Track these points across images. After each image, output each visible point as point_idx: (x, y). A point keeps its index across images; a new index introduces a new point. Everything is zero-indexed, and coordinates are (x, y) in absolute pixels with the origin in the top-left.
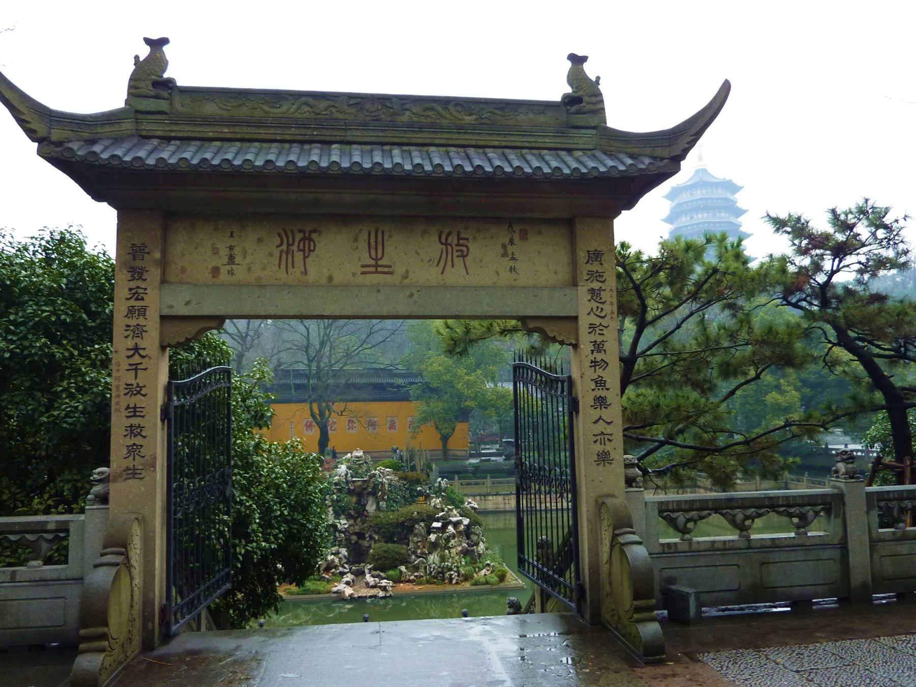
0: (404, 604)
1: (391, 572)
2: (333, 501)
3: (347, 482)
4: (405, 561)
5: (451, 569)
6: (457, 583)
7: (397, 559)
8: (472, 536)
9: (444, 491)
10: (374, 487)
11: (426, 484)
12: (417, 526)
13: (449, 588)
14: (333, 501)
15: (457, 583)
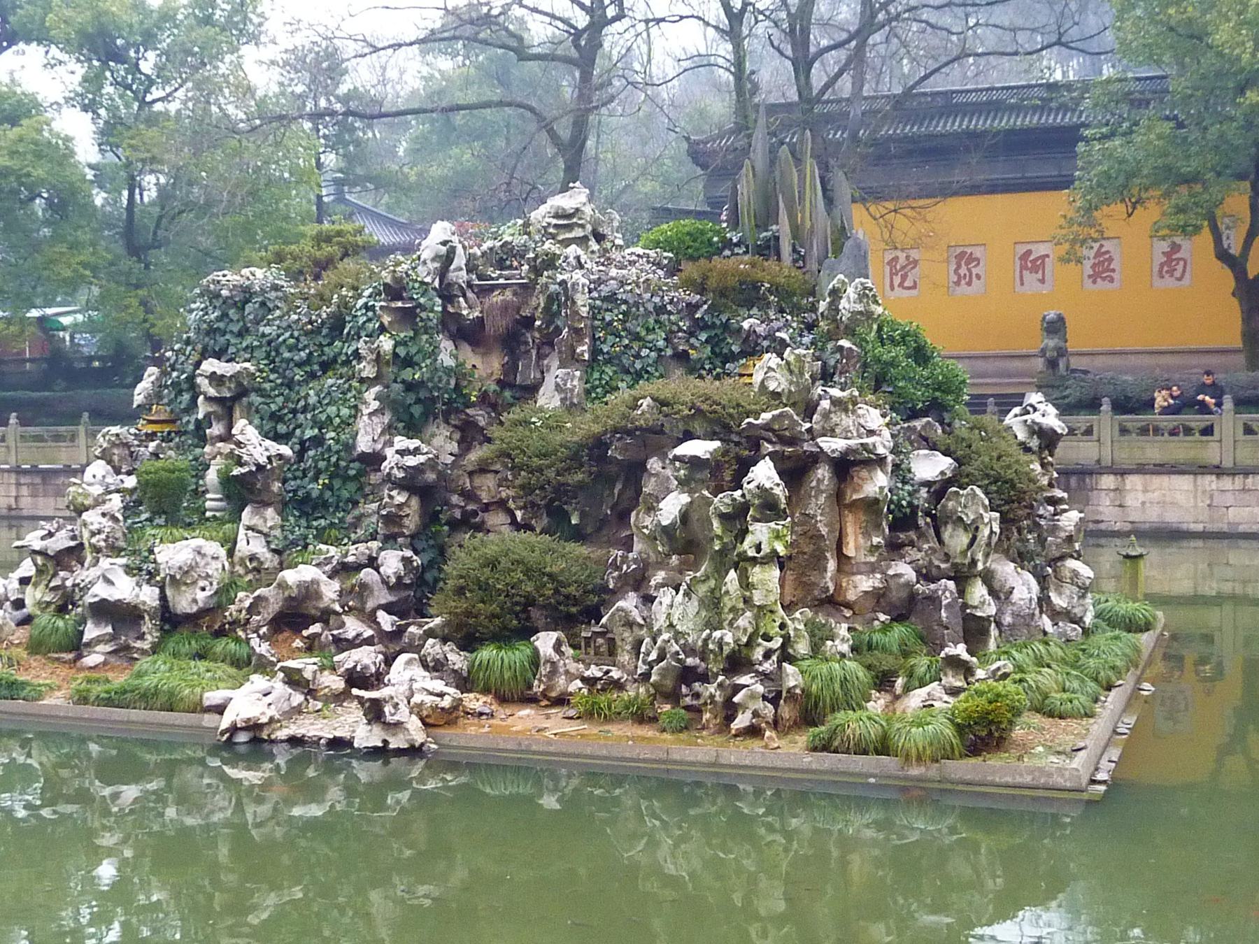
0: (550, 802)
1: (487, 653)
2: (379, 359)
3: (447, 293)
4: (578, 612)
5: (737, 662)
6: (753, 731)
7: (530, 602)
8: (947, 533)
9: (850, 332)
10: (547, 309)
11: (796, 310)
12: (654, 464)
13: (701, 749)
14: (379, 359)
15: (753, 731)
